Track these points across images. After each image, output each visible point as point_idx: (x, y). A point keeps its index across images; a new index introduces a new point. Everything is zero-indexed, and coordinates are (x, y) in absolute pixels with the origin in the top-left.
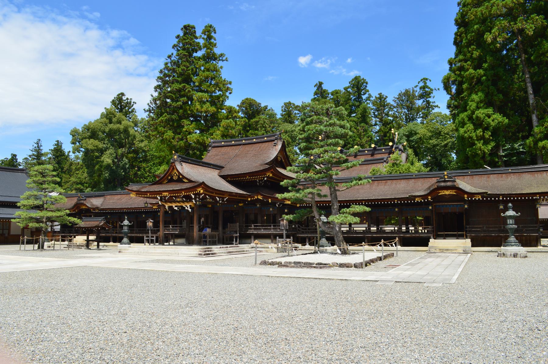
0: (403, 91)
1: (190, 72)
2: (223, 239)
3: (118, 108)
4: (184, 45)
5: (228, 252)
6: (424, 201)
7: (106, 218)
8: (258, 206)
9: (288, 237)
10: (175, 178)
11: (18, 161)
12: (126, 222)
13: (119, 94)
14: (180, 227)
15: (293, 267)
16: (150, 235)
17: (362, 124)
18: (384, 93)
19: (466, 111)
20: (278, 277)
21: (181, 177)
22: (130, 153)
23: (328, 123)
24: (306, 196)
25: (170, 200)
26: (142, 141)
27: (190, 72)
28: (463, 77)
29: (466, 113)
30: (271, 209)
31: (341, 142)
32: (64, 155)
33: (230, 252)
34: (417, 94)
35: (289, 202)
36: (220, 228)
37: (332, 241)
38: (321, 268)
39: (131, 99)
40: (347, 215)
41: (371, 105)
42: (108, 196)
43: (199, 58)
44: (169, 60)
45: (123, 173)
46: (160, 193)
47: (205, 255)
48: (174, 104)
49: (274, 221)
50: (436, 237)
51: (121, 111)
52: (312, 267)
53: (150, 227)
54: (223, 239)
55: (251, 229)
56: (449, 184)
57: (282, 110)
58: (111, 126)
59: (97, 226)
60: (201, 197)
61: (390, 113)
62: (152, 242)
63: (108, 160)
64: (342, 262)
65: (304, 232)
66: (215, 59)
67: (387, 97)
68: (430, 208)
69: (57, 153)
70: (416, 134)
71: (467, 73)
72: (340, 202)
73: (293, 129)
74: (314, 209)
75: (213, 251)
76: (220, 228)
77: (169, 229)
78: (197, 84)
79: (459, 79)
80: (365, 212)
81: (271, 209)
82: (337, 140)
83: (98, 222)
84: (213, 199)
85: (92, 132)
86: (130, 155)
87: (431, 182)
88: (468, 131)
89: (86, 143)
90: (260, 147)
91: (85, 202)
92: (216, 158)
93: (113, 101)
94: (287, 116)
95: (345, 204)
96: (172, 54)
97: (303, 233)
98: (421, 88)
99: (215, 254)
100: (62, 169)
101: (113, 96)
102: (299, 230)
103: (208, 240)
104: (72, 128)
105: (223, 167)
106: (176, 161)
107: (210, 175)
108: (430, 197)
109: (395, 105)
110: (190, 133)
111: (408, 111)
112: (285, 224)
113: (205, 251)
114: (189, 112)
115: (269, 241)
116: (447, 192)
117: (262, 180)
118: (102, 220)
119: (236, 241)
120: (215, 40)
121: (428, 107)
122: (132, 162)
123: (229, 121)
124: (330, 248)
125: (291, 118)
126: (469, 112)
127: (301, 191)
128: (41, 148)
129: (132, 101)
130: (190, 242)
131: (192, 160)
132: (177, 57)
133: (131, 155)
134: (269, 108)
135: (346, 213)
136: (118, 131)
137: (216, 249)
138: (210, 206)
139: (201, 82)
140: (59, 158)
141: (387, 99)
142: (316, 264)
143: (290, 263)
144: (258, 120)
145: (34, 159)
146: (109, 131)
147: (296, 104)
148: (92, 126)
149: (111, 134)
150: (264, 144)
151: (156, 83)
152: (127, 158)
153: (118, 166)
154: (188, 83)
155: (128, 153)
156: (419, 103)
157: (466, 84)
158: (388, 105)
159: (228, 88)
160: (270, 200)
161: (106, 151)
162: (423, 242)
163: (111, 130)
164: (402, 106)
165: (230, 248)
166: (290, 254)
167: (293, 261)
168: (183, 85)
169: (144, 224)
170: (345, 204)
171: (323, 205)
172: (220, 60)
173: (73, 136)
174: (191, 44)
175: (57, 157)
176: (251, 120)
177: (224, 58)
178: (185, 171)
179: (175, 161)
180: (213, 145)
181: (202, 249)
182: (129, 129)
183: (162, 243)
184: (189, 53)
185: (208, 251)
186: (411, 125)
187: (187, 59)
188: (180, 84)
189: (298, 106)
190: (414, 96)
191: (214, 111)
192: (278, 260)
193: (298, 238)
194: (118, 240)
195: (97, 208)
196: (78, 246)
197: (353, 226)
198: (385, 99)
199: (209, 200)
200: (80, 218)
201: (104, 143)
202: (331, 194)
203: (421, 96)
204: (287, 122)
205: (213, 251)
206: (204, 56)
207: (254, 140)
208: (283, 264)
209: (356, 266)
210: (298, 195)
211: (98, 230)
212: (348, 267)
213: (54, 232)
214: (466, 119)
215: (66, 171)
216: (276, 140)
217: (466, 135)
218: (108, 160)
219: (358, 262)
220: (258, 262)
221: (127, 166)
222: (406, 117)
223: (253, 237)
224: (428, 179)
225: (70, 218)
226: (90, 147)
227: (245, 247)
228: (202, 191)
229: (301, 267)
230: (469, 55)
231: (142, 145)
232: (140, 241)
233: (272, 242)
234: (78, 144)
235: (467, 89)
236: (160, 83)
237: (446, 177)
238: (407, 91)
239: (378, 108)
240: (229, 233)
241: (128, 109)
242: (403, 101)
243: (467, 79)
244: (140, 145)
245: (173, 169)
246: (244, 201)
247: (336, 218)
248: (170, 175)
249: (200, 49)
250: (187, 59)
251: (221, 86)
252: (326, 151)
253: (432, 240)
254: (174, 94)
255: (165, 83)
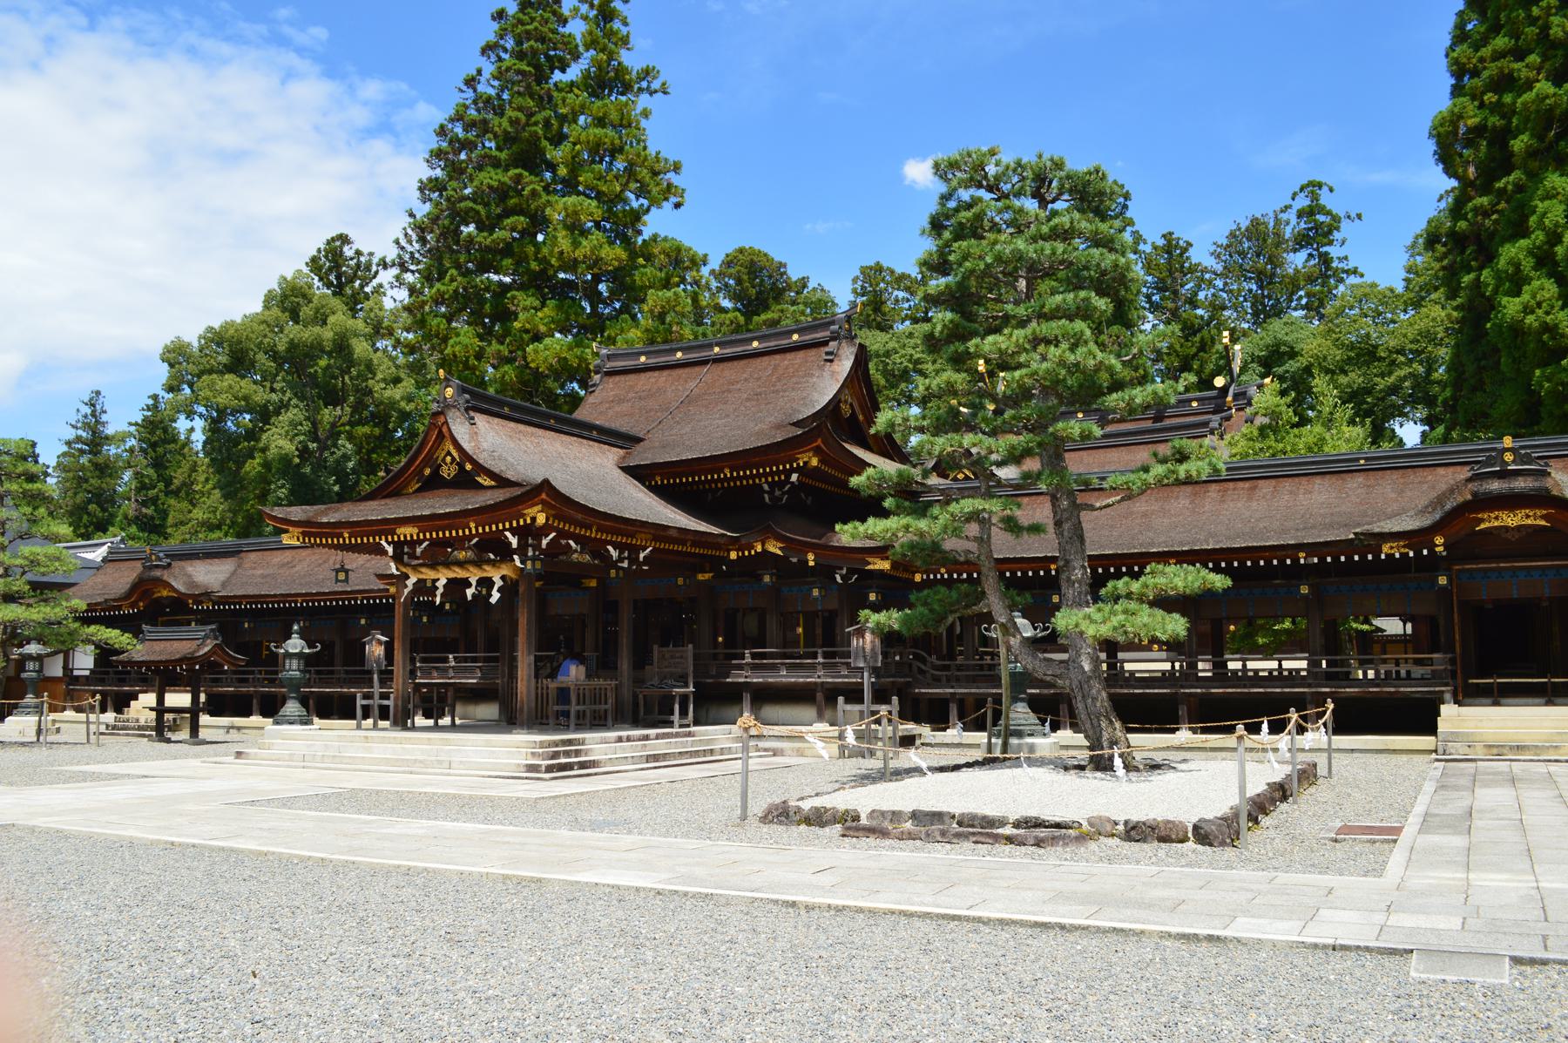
0: (1245, 224)
1: (539, 130)
2: (636, 704)
3: (329, 285)
4: (519, 43)
5: (649, 758)
6: (1418, 553)
7: (222, 630)
8: (767, 579)
9: (881, 696)
10: (448, 472)
11: (41, 460)
12: (295, 644)
13: (333, 239)
14: (486, 660)
15: (911, 836)
16: (377, 689)
17: (1115, 329)
18: (1183, 234)
19: (1525, 233)
20: (840, 910)
21: (468, 467)
22: (361, 422)
23: (1045, 229)
24: (956, 533)
25: (438, 555)
26: (397, 381)
27: (539, 130)
28: (1506, 112)
29: (1523, 243)
30: (816, 592)
31: (1102, 304)
32: (174, 439)
33: (656, 758)
34: (1288, 232)
35: (885, 565)
36: (625, 665)
37: (1054, 709)
38: (1038, 843)
39: (371, 254)
40: (1133, 605)
41: (1138, 270)
42: (253, 556)
43: (572, 84)
44: (470, 94)
45: (336, 488)
46: (386, 527)
47: (549, 769)
48: (484, 239)
49: (829, 636)
50: (1466, 695)
51: (339, 291)
52: (997, 838)
53: (378, 661)
54: (636, 704)
55: (740, 667)
56: (1520, 484)
57: (855, 291)
58: (293, 331)
59: (189, 659)
60: (544, 542)
61: (1201, 295)
62: (384, 714)
63: (281, 442)
64: (1136, 816)
65: (944, 678)
66: (627, 88)
67: (1189, 245)
68: (1443, 580)
69: (152, 433)
70: (1293, 354)
71: (1528, 96)
72: (1095, 560)
73: (891, 345)
74: (991, 585)
75: (587, 753)
76: (625, 665)
77: (446, 670)
78: (563, 171)
79: (1495, 121)
80: (1208, 595)
81: (816, 592)
82: (1082, 294)
83: (193, 642)
84: (594, 555)
85: (232, 351)
86: (362, 430)
87: (1448, 481)
88: (1539, 305)
89: (211, 386)
90: (776, 368)
91: (166, 576)
92: (617, 409)
93: (314, 260)
94: (869, 310)
95: (1110, 569)
96: (479, 72)
97: (937, 681)
98: (1300, 214)
99: (593, 764)
100: (168, 482)
101: (314, 243)
102: (921, 672)
103: (574, 708)
104: (167, 339)
105: (639, 440)
106: (448, 406)
107: (584, 465)
108: (1439, 540)
109: (1219, 268)
110: (537, 338)
111: (1261, 287)
112: (868, 647)
113: (555, 755)
114: (534, 265)
115: (809, 712)
116: (1511, 519)
117: (781, 484)
118: (206, 637)
119: (684, 713)
120: (626, 24)
121: (1325, 277)
122: (370, 452)
123: (669, 294)
124: (1049, 742)
125: (884, 314)
126: (1539, 237)
127: (936, 510)
128: (104, 418)
129: (375, 260)
130: (510, 720)
131: (513, 407)
132: (496, 83)
133: (366, 429)
134: (811, 285)
135: (1129, 596)
136: (315, 350)
137: (598, 744)
138: (593, 583)
139: (575, 166)
140: (160, 450)
141: (1191, 252)
142: (1017, 825)
143: (896, 816)
144: (776, 316)
145: (82, 452)
146: (288, 350)
147: (899, 270)
148: (231, 332)
149: (296, 359)
150: (789, 356)
151: (426, 173)
152: (350, 438)
153: (320, 465)
154: (534, 169)
155: (352, 424)
156: (1297, 260)
157: (1525, 137)
158: (1192, 270)
159: (669, 185)
160: (811, 557)
161: (278, 414)
162: (1420, 719)
163: (293, 346)
164: (1243, 274)
165: (658, 741)
166: (893, 764)
167: (908, 807)
168: (512, 172)
169: (356, 653)
170: (1110, 569)
171: (1025, 573)
172: (640, 90)
173: (171, 366)
174: (542, 40)
175: (154, 445)
176: (756, 318)
177: (656, 85)
178: (485, 445)
179: (446, 406)
180: (609, 365)
181: (542, 744)
182: (353, 341)
183: (402, 721)
184: (538, 67)
185: (567, 754)
186: (1276, 327)
187: (528, 87)
188: (506, 170)
189: (903, 277)
190: (1279, 241)
191: (618, 259)
192: (841, 801)
193: (917, 700)
194: (270, 708)
195: (207, 595)
196: (140, 728)
197: (1121, 655)
198: (1186, 250)
199: (579, 556)
200: (137, 632)
201: (273, 390)
202: (1058, 524)
203: (1302, 241)
204: (869, 327)
205: (587, 753)
206: (586, 75)
207: (717, 349)
208: (864, 821)
209: (1202, 835)
210: (923, 524)
211: (191, 670)
212: (1164, 839)
213: (69, 677)
214: (1527, 264)
215: (179, 490)
216: (833, 339)
217: (1530, 319)
218: (281, 442)
219: (1210, 816)
220: (757, 807)
221: (351, 465)
222: (1253, 305)
223: (747, 698)
224: (1420, 472)
225: (93, 629)
226: (222, 400)
227: (716, 735)
228: (541, 519)
229: (946, 837)
230: (1531, 31)
231: (396, 393)
232: (339, 708)
233: (820, 717)
234: (187, 391)
235: (1531, 153)
236: (438, 173)
237: (1508, 457)
238: (1255, 223)
239: (1162, 280)
240: (656, 681)
241: (362, 287)
242: (1242, 254)
243: (1527, 120)
244: (388, 393)
245: (441, 436)
246: (714, 563)
247: (1083, 621)
248: (429, 459)
249: (576, 57)
250: (528, 87)
251: (644, 173)
252: (1036, 341)
253: (1448, 711)
254: (486, 205)
255: (455, 170)
